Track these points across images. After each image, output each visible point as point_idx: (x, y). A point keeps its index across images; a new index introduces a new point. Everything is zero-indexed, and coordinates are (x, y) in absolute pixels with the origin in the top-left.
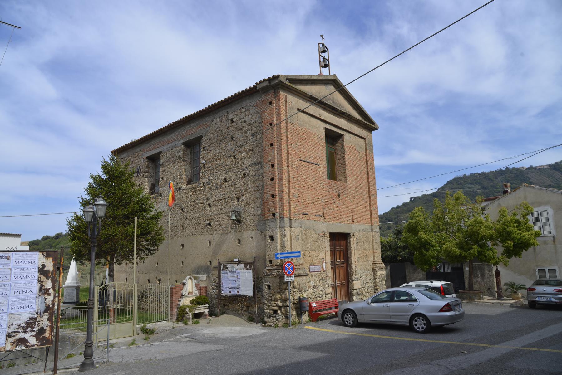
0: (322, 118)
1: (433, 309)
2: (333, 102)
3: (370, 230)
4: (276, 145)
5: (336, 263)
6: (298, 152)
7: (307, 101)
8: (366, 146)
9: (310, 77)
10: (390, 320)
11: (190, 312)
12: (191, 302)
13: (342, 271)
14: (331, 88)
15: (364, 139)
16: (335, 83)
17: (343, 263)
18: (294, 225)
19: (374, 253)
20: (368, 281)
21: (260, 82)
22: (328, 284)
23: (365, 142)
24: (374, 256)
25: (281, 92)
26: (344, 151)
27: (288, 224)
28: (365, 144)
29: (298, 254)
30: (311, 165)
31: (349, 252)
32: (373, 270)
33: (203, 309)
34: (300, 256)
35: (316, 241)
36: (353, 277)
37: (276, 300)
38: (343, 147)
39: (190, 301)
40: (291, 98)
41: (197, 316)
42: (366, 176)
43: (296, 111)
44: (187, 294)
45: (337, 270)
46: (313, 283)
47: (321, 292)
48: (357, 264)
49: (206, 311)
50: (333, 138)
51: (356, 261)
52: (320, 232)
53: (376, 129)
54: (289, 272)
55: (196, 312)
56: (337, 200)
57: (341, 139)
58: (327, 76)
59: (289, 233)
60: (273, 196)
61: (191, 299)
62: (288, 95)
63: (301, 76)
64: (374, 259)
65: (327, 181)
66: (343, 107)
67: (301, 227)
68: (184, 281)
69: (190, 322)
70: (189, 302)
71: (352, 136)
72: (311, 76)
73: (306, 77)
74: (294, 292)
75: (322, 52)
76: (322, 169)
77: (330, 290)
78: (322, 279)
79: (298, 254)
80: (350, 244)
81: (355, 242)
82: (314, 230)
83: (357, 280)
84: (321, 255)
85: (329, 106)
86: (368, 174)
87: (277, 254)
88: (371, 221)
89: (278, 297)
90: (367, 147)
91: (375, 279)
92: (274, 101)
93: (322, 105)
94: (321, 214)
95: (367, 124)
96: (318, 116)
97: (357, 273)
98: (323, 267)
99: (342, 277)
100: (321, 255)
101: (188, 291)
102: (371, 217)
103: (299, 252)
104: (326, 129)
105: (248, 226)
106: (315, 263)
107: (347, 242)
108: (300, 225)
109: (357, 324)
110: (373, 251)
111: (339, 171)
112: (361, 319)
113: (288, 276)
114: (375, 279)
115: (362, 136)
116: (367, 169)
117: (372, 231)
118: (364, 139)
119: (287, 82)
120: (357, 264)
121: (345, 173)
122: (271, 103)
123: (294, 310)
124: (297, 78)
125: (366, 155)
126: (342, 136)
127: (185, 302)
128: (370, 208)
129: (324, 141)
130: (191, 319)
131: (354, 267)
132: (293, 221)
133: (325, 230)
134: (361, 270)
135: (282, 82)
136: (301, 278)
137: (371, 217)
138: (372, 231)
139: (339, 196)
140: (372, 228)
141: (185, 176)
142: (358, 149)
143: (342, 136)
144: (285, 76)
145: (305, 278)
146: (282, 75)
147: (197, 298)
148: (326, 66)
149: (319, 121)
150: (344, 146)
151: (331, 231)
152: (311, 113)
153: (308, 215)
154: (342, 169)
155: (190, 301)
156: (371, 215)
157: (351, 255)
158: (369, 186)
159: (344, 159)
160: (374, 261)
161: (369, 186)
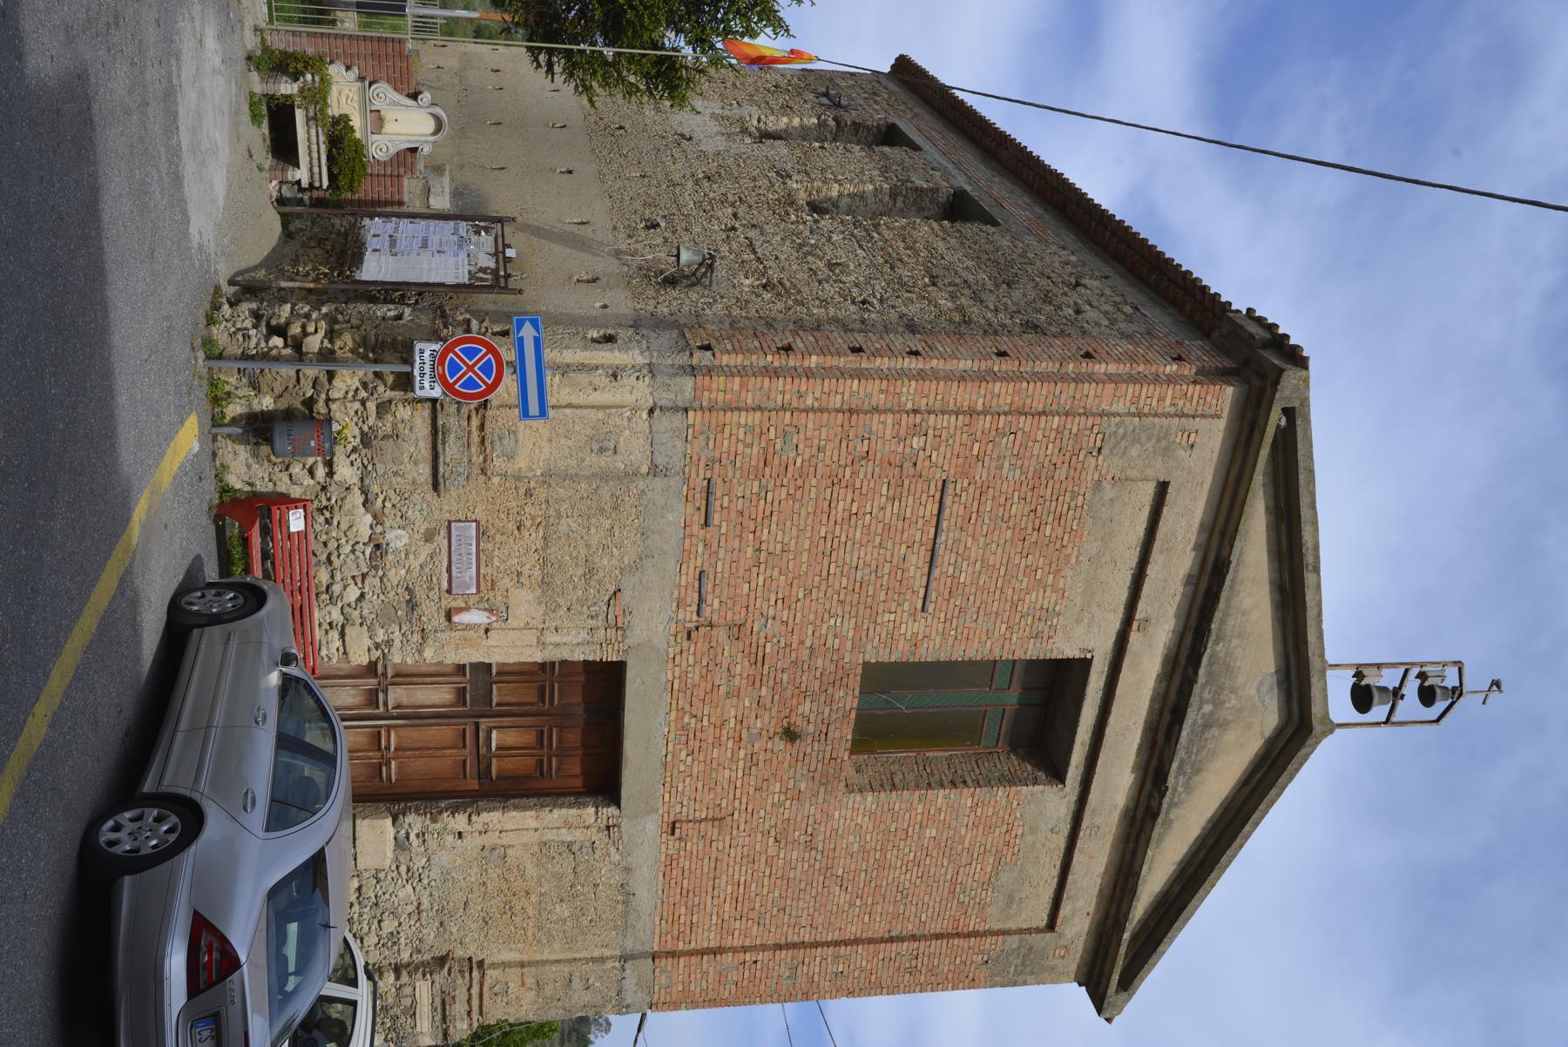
0: (1134, 637)
1: (217, 883)
2: (1207, 726)
3: (630, 945)
4: (999, 366)
5: (485, 723)
6: (980, 474)
7: (1203, 549)
8: (1020, 931)
9: (1309, 559)
10: (183, 726)
11: (301, 90)
12: (342, 121)
13: (443, 764)
14: (1268, 717)
15: (1051, 925)
16: (1295, 734)
17: (483, 774)
18: (664, 422)
19: (522, 965)
20: (389, 925)
21: (1261, 321)
22: (389, 643)
23: (1038, 930)
24: (505, 965)
25: (1230, 391)
26: (989, 783)
27: (665, 398)
28: (1029, 931)
29: (534, 408)
30: (924, 555)
31: (533, 801)
32: (441, 961)
33: (310, 167)
34: (525, 414)
35: (590, 572)
36: (411, 818)
37: (331, 335)
38: (1010, 780)
39: (344, 119)
40: (1212, 437)
41: (280, 120)
42: (879, 929)
43: (1158, 472)
44: (377, 105)
45: (445, 733)
46: (397, 538)
47: (352, 594)
48: (472, 842)
49: (302, 174)
50: (1041, 715)
51: (488, 840)
52: (625, 598)
53: (1099, 1002)
54: (454, 368)
55: (300, 115)
56: (768, 721)
57: (1042, 775)
58: (1322, 655)
59: (629, 399)
60: (788, 349)
61: (356, 122)
62: (1221, 424)
63: (1312, 495)
64: (493, 966)
65: (854, 660)
66: (1188, 788)
67: (654, 470)
68: (426, 97)
69: (257, 84)
70: (345, 110)
71: (1060, 841)
72: (1317, 570)
73: (1307, 536)
74: (363, 402)
75: (1422, 676)
76: (909, 628)
77: (360, 656)
78: (412, 605)
79: (534, 408)
80: (570, 806)
81: (578, 835)
82: (635, 567)
83: (401, 845)
84: (524, 603)
85: (1188, 683)
86: (891, 940)
87: (535, 324)
88: (673, 954)
89: (347, 340)
90: (1014, 941)
91: (397, 969)
92: (1188, 370)
93: (1188, 641)
94: (707, 611)
95: (1114, 962)
96: (1140, 614)
97: (432, 843)
98: (467, 609)
99: (418, 765)
100: (524, 603)
101: (388, 114)
102: (690, 953)
103: (543, 413)
104: (1084, 665)
105: (652, 302)
106: (490, 558)
107: (578, 794)
108: (660, 460)
109: (180, 630)
110: (531, 964)
111: (898, 759)
112: (207, 646)
113: (438, 359)
114: (397, 969)
115: (1065, 910)
116: (914, 938)
117: (624, 958)
118: (1051, 925)
119: (1276, 419)
120: (472, 842)
121: (894, 787)
122: (1179, 359)
123: (283, 404)
124: (1302, 477)
125: (975, 934)
126: (1057, 774)
127: (345, 93)
128: (734, 950)
129: (1034, 651)
130: (270, 89)
131: (460, 822)
132: (678, 420)
133: (638, 634)
134: (446, 875)
135: (1276, 382)
136: (424, 450)
137: (690, 953)
138: (624, 958)
139: (790, 735)
140: (642, 955)
141: (835, 194)
142: (1004, 878)
143: (1057, 774)
144: (1305, 402)
145: (425, 470)
146: (1306, 380)
147: (359, 148)
148: (1362, 697)
149: (1115, 624)
150: (1011, 783)
151: (631, 675)
152: (1152, 570)
153: (706, 524)
154: (910, 777)
155: (344, 119)
156: (702, 953)
157: (516, 808)
158: (837, 944)
159: (953, 784)
160: (481, 964)
161: (837, 944)
